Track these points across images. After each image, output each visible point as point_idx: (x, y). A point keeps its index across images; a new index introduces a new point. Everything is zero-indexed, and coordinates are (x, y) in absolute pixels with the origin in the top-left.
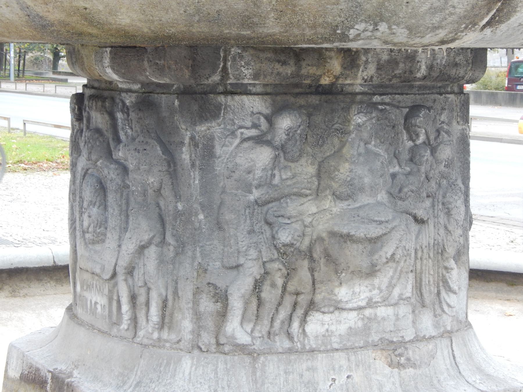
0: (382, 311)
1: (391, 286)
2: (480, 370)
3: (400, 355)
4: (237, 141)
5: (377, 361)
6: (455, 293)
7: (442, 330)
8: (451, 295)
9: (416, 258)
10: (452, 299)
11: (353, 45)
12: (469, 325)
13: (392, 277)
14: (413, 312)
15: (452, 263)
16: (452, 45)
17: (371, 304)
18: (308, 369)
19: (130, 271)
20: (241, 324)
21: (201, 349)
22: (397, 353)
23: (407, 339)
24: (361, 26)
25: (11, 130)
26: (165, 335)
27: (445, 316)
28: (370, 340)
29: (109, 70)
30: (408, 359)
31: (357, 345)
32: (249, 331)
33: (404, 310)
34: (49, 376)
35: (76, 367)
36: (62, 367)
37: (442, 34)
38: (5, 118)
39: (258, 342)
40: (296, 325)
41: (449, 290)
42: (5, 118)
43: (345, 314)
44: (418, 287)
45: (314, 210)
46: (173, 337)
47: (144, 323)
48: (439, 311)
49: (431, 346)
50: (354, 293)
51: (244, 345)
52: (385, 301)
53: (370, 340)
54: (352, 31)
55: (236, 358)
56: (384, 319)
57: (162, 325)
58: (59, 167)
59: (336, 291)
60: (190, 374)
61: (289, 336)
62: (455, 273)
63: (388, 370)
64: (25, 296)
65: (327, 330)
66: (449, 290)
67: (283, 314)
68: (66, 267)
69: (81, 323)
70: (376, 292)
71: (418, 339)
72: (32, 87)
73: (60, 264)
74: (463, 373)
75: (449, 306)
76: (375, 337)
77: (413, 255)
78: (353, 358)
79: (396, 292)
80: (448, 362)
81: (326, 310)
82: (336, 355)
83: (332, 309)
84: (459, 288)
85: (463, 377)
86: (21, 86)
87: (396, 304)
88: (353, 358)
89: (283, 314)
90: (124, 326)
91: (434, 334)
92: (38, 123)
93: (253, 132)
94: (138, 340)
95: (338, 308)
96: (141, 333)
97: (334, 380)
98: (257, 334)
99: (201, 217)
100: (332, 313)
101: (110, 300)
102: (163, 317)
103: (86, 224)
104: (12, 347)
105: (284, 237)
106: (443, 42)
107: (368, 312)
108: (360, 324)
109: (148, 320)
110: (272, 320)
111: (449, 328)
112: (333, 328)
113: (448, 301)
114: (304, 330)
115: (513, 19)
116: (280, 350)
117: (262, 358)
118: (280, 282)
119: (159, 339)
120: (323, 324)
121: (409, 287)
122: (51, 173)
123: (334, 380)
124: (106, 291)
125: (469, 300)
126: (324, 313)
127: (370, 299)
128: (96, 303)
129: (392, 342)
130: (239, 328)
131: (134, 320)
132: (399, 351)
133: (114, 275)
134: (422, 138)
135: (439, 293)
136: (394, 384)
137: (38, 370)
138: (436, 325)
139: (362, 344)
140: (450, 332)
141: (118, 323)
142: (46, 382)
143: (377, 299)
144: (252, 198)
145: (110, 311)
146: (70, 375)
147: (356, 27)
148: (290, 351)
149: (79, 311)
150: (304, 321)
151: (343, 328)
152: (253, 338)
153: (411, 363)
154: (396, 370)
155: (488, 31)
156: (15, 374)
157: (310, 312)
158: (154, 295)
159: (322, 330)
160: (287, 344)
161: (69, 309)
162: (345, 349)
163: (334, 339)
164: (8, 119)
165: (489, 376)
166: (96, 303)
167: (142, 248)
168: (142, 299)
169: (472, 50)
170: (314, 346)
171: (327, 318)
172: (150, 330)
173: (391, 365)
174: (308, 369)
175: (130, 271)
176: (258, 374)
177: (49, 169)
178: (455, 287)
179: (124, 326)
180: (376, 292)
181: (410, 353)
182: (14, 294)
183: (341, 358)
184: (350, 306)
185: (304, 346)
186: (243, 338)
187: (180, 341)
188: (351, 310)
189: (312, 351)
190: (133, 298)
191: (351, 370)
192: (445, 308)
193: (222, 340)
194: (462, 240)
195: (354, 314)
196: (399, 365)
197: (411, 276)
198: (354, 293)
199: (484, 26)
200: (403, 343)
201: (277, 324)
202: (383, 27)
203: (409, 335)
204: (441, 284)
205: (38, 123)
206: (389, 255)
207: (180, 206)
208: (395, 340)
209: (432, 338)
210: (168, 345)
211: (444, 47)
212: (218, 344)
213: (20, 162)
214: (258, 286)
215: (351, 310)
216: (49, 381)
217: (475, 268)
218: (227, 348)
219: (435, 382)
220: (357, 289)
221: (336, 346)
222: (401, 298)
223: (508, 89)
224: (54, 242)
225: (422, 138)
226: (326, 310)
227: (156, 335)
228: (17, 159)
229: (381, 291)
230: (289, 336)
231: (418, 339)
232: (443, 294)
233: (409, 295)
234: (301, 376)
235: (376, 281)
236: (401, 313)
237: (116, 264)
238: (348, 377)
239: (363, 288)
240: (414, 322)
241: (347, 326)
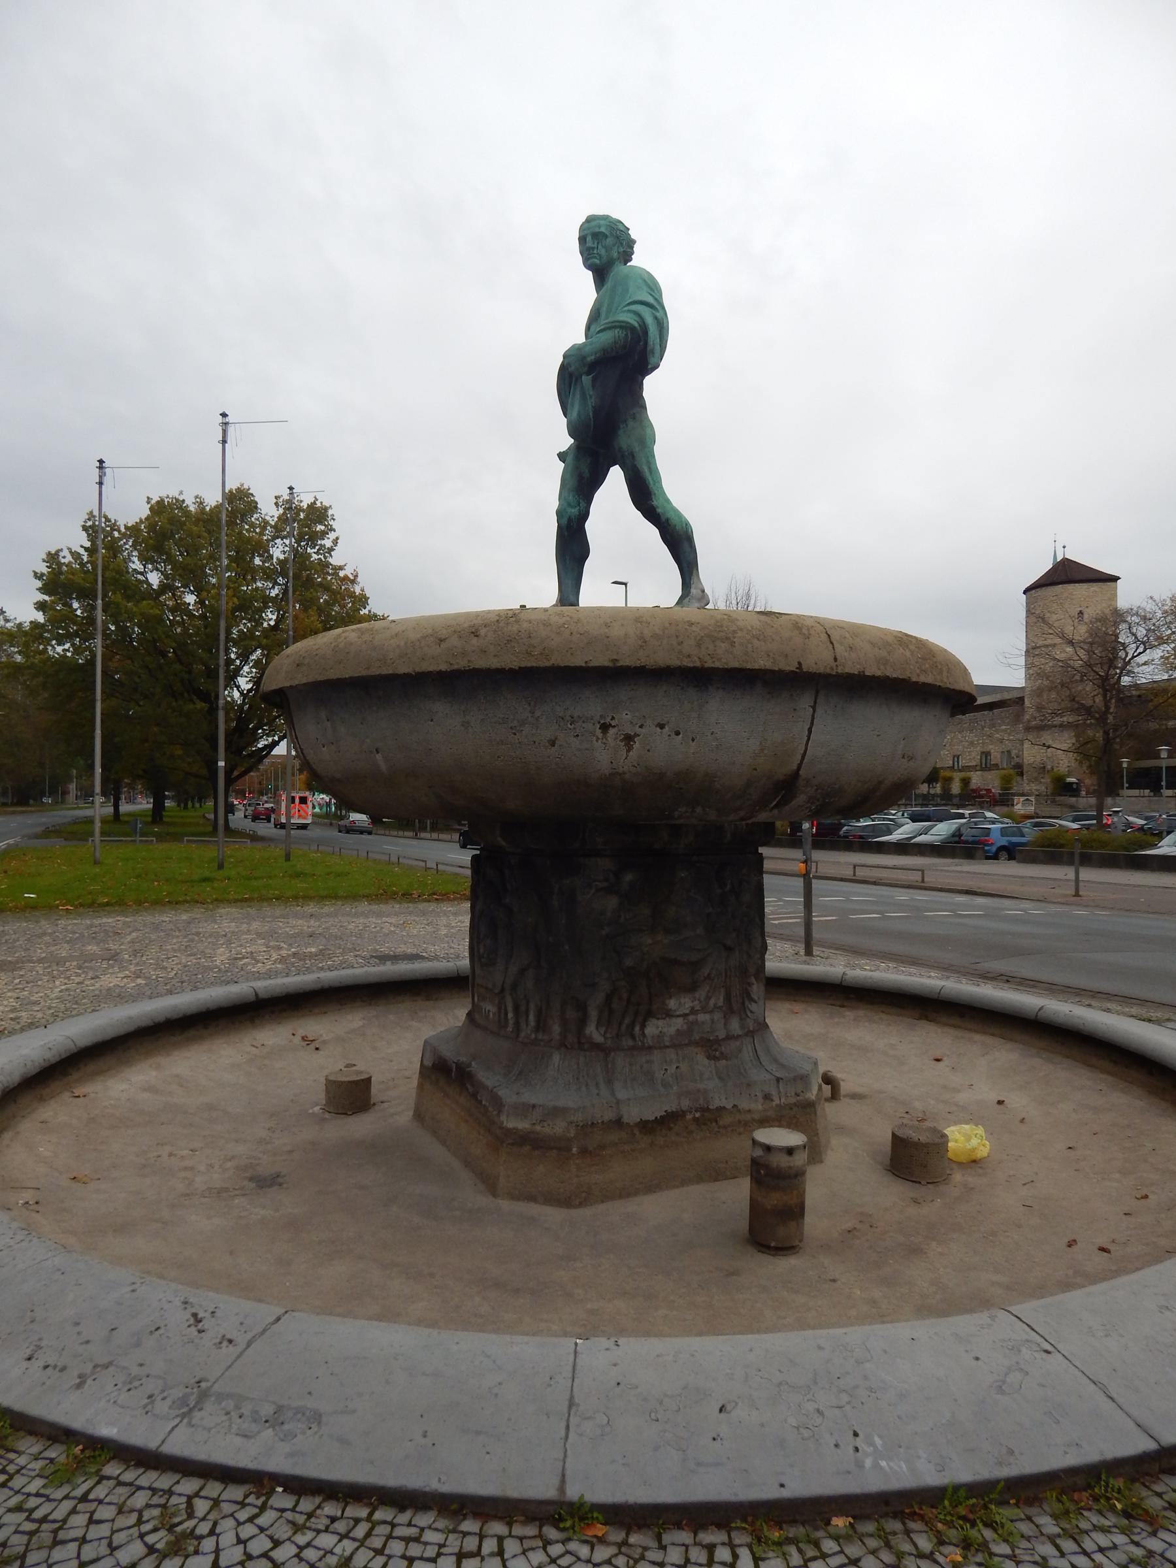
0: (702, 1017)
1: (708, 998)
2: (776, 1061)
3: (716, 1050)
4: (593, 891)
5: (698, 1055)
6: (756, 1002)
7: (746, 1030)
8: (753, 1003)
9: (726, 976)
10: (753, 1007)
11: (678, 822)
12: (767, 1026)
13: (709, 991)
14: (725, 1017)
15: (753, 980)
16: (750, 822)
17: (693, 1011)
18: (647, 1062)
19: (514, 987)
20: (597, 1029)
21: (566, 1046)
22: (713, 1048)
23: (720, 1038)
24: (682, 809)
25: (427, 869)
26: (540, 1036)
27: (748, 1020)
28: (693, 1039)
29: (499, 839)
30: (722, 1053)
31: (683, 1043)
32: (602, 1032)
33: (718, 1016)
34: (454, 1065)
35: (474, 1059)
36: (463, 1059)
37: (742, 813)
38: (423, 861)
39: (609, 1042)
40: (637, 1029)
41: (752, 1000)
42: (423, 861)
43: (674, 1020)
44: (728, 998)
45: (650, 941)
46: (546, 1037)
47: (525, 1026)
48: (744, 1016)
49: (738, 1043)
50: (680, 1003)
51: (598, 1044)
52: (704, 1009)
53: (693, 1039)
54: (676, 813)
55: (593, 1053)
56: (703, 1023)
57: (537, 1029)
58: (463, 898)
59: (667, 1002)
60: (559, 1066)
61: (633, 1037)
62: (755, 987)
63: (706, 1061)
64: (436, 999)
65: (661, 1032)
66: (752, 1000)
67: (627, 1021)
68: (467, 978)
69: (478, 1026)
70: (697, 1002)
71: (730, 1037)
72: (442, 836)
73: (462, 975)
74: (763, 1063)
75: (751, 1012)
76: (697, 1037)
77: (724, 975)
78: (680, 1052)
79: (712, 1002)
80: (751, 1054)
81: (660, 1016)
82: (668, 1050)
83: (664, 1016)
84: (759, 998)
85: (763, 1066)
86: (435, 835)
87: (711, 1012)
88: (680, 1052)
89: (627, 1021)
90: (510, 1029)
91: (740, 1033)
92: (447, 865)
93: (605, 884)
94: (520, 1039)
95: (668, 1014)
96: (523, 1034)
97: (666, 1070)
98: (608, 1035)
99: (567, 947)
100: (664, 1019)
101: (500, 1009)
102: (538, 1021)
103: (482, 951)
104: (426, 1042)
105: (629, 962)
106: (743, 819)
107: (691, 1018)
108: (685, 1027)
109: (527, 1025)
110: (620, 1024)
111: (751, 1029)
112: (665, 1030)
113: (751, 1009)
114: (643, 1032)
115: (793, 803)
116: (626, 1047)
117: (612, 1054)
118: (625, 996)
119: (536, 1038)
120: (658, 1027)
121: (722, 999)
122: (456, 903)
123: (666, 1070)
124: (497, 1002)
125: (767, 1004)
126: (658, 1019)
127: (692, 1008)
128: (489, 1011)
129: (709, 1040)
130: (595, 1031)
131: (517, 1024)
132: (715, 1047)
133: (502, 990)
134: (729, 887)
135: (743, 1003)
136: (711, 1072)
137: (445, 1060)
138: (742, 1027)
139: (687, 1042)
140: (752, 1032)
141: (506, 1026)
142: (451, 1070)
143: (698, 1008)
144: (604, 933)
145: (499, 1016)
146: (470, 1065)
147: (680, 810)
148: (633, 1048)
149: (477, 1016)
150: (643, 1026)
151: (672, 1030)
152: (606, 1038)
153: (723, 1056)
154: (713, 1061)
155: (776, 812)
156: (428, 1063)
157: (647, 1023)
158: (532, 1006)
159: (657, 1032)
160: (631, 1043)
161: (469, 1014)
162: (674, 1046)
163: (666, 1038)
164: (425, 861)
165: (783, 1066)
166: (489, 1011)
167: (522, 972)
168: (523, 1008)
169: (764, 823)
170: (651, 1044)
171: (660, 1023)
172: (529, 1032)
173: (709, 1058)
174: (647, 1062)
175: (514, 987)
176: (610, 1066)
177: (455, 899)
178: (755, 997)
179: (510, 1029)
180: (697, 1002)
181: (723, 1049)
182: (428, 998)
183: (671, 1054)
184: (678, 1013)
185: (643, 1042)
186: (598, 1038)
187: (552, 1040)
188: (678, 1016)
189: (650, 1048)
190: (516, 1008)
191: (679, 1062)
192: (749, 1014)
193: (583, 1040)
194: (760, 962)
195: (680, 1020)
196: (715, 1058)
197: (723, 990)
198: (680, 1003)
199: (773, 808)
200: (717, 1041)
201: (624, 1027)
202: (699, 810)
203: (722, 1034)
204: (745, 995)
205: (447, 865)
206: (706, 975)
207: (551, 939)
208: (711, 1038)
209: (739, 1036)
210: (542, 1043)
211: (744, 822)
212: (579, 1043)
213: (434, 894)
214: (609, 998)
215: (678, 1016)
216: (454, 1070)
217: (769, 976)
218: (586, 1046)
219: (742, 1071)
220: (683, 1001)
221: (667, 1044)
222: (715, 1006)
223: (790, 835)
224: (458, 957)
225: (729, 887)
226: (660, 1016)
227: (533, 1036)
228: (431, 892)
229: (700, 1002)
230: (633, 1037)
231: (730, 1037)
232: (747, 1003)
233: (721, 1004)
234: (641, 1067)
235: (697, 995)
236: (716, 1018)
237: (504, 982)
238: (677, 1067)
239: (687, 1000)
240: (725, 1024)
241: (676, 1028)
